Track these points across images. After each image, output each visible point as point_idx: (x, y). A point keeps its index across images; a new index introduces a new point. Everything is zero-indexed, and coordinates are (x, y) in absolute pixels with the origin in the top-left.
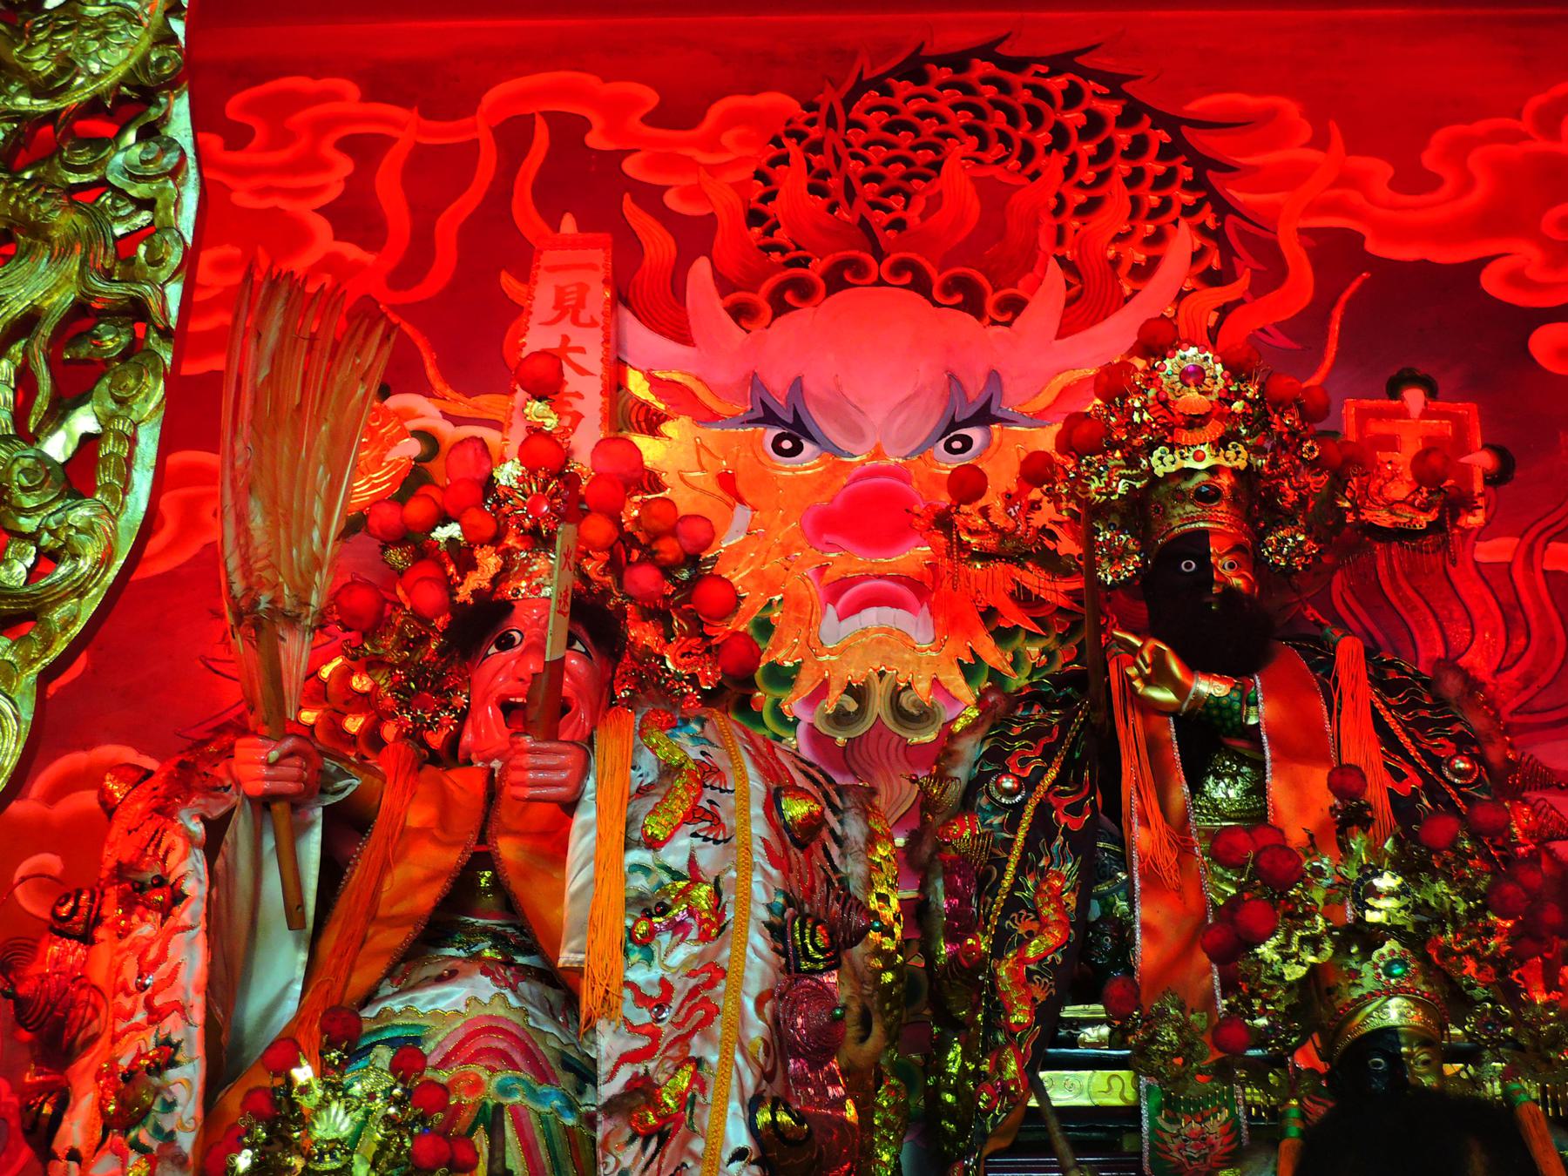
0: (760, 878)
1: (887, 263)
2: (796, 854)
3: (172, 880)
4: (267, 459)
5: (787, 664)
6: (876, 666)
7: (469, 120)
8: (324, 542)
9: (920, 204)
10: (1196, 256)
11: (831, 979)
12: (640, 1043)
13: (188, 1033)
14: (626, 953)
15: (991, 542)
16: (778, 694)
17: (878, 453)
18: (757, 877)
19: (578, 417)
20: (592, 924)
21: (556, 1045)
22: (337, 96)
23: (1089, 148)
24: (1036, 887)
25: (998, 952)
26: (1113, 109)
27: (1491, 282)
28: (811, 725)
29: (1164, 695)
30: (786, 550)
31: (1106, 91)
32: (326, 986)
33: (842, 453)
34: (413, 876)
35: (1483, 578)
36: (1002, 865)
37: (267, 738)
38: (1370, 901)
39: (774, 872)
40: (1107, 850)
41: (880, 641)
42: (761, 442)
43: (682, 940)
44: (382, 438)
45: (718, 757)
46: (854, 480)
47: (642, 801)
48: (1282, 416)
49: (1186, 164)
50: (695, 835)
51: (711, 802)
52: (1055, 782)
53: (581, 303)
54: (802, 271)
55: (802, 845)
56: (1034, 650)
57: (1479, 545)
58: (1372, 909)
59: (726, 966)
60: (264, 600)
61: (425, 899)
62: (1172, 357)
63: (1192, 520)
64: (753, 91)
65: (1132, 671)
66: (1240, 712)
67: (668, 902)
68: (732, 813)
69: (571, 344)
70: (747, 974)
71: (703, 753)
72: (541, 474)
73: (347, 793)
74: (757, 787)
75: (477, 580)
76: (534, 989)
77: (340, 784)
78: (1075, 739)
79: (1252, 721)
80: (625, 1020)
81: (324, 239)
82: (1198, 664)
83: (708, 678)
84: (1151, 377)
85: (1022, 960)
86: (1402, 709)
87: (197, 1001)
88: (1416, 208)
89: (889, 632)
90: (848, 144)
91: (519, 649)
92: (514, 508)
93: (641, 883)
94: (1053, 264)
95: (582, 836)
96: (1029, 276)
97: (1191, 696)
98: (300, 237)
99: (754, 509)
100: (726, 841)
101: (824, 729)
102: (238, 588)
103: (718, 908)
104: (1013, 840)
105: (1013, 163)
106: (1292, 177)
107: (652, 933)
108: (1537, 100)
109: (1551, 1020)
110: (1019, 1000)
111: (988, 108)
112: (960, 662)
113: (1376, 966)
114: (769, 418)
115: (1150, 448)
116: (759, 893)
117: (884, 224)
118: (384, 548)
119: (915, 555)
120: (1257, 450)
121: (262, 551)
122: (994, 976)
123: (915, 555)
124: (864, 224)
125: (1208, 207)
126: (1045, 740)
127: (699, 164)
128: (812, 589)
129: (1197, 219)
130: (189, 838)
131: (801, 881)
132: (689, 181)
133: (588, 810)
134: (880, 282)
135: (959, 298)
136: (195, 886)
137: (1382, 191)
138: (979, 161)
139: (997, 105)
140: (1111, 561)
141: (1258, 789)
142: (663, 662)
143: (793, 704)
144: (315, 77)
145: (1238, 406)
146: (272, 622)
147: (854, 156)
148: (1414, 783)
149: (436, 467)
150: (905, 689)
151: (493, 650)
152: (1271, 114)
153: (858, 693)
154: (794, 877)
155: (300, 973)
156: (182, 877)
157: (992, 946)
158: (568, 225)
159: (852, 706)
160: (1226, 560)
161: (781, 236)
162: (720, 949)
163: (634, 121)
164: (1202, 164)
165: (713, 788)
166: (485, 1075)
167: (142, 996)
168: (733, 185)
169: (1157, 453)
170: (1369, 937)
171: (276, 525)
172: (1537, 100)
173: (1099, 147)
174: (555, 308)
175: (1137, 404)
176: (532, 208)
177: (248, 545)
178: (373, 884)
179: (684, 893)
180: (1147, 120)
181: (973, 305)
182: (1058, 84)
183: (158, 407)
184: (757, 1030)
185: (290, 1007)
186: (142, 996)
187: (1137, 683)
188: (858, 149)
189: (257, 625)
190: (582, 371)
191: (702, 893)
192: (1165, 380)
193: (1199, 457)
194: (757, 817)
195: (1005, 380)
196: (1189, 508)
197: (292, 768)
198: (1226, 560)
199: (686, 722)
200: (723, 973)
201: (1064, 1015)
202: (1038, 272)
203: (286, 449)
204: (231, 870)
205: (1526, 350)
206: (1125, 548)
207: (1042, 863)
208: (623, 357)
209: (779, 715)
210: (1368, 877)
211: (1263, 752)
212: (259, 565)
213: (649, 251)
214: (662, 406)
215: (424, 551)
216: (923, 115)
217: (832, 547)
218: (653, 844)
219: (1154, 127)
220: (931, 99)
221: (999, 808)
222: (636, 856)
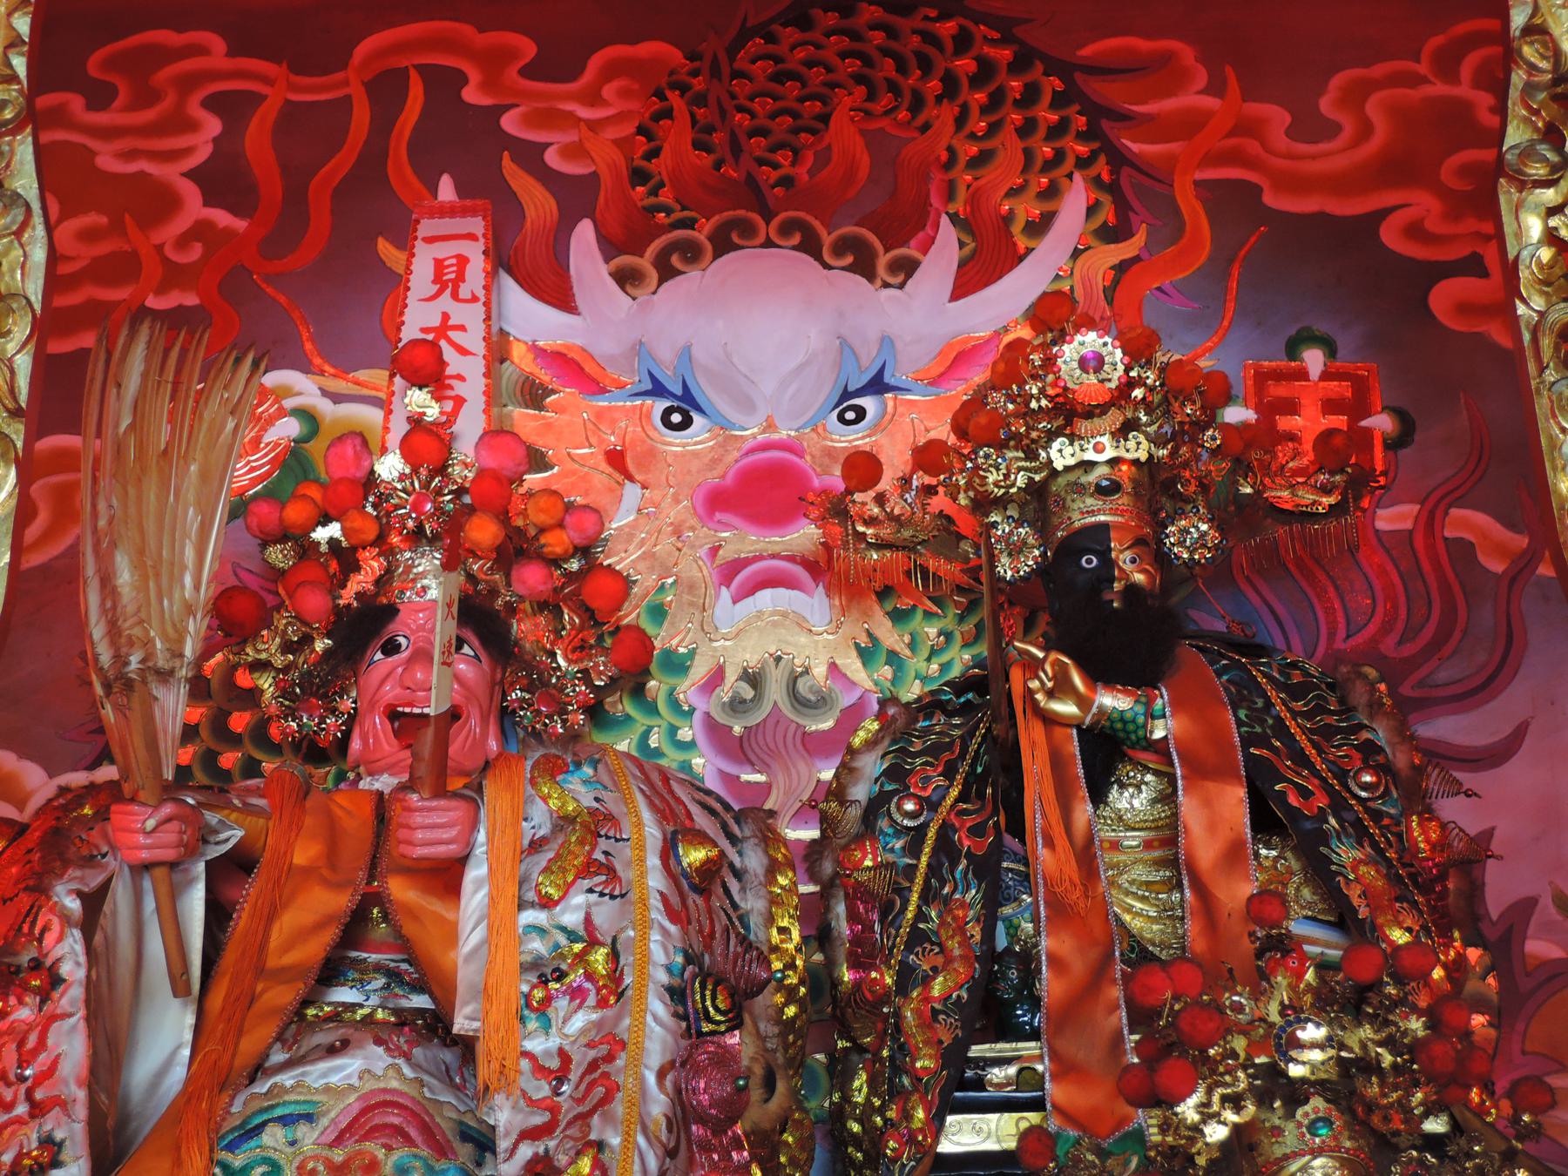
0: (658, 937)
1: (775, 222)
2: (695, 899)
3: (48, 962)
4: (132, 510)
5: (682, 650)
6: (772, 650)
7: (339, 76)
8: (197, 587)
9: (809, 158)
10: (1091, 210)
11: (734, 1039)
12: (539, 1119)
13: (71, 1130)
14: (522, 1020)
15: (886, 532)
16: (672, 681)
17: (770, 426)
18: (655, 936)
19: (459, 401)
20: (485, 993)
21: (454, 1115)
22: (202, 51)
23: (980, 96)
24: (940, 916)
25: (903, 987)
26: (1005, 54)
27: (1390, 236)
28: (707, 715)
29: (1066, 708)
30: (677, 532)
31: (997, 36)
32: (214, 1057)
33: (733, 426)
34: (303, 921)
35: (1384, 547)
36: (904, 893)
37: (144, 804)
38: (1293, 1053)
39: (673, 928)
40: (1011, 870)
41: (775, 624)
42: (649, 415)
43: (580, 1006)
44: (260, 418)
45: (612, 803)
46: (747, 454)
47: (536, 858)
48: (1183, 405)
49: (1079, 113)
50: (591, 891)
51: (606, 853)
52: (957, 800)
53: (461, 277)
54: (689, 232)
55: (703, 891)
56: (932, 631)
57: (1380, 512)
58: (1296, 1061)
59: (625, 1037)
60: (134, 661)
61: (314, 949)
62: (1071, 342)
63: (1092, 513)
64: (634, 41)
65: (1034, 684)
66: (1145, 726)
67: (564, 967)
68: (628, 864)
69: (451, 323)
70: (648, 1044)
71: (597, 799)
72: (423, 472)
73: (229, 845)
74: (653, 832)
75: (360, 582)
76: (429, 1054)
77: (223, 836)
78: (977, 752)
79: (1159, 734)
80: (524, 1093)
81: (194, 208)
82: (1102, 673)
83: (601, 673)
84: (1050, 362)
85: (926, 999)
86: (1308, 715)
87: (81, 1095)
88: (1314, 157)
89: (784, 615)
90: (733, 97)
91: (404, 655)
92: (397, 507)
93: (537, 946)
94: (945, 220)
95: (476, 892)
96: (921, 235)
97: (1094, 710)
98: (164, 202)
99: (644, 487)
100: (622, 896)
101: (721, 718)
102: (105, 658)
103: (615, 976)
104: (916, 867)
105: (903, 115)
106: (1188, 125)
107: (548, 1000)
108: (1437, 41)
109: (1477, 1155)
110: (926, 1043)
111: (876, 55)
112: (857, 645)
113: (1300, 1125)
114: (658, 390)
115: (1051, 436)
116: (658, 953)
117: (772, 181)
118: (264, 545)
119: (805, 535)
120: (1157, 441)
121: (130, 609)
122: (898, 1014)
123: (805, 535)
124: (750, 180)
125: (1102, 159)
126: (946, 756)
127: (580, 119)
128: (705, 572)
129: (1093, 171)
130: (66, 919)
131: (701, 931)
132: (571, 137)
133: (479, 866)
134: (769, 244)
135: (849, 260)
136: (73, 968)
137: (1280, 141)
138: (867, 113)
139: (886, 52)
140: (1010, 555)
141: (1167, 797)
142: (553, 655)
143: (687, 688)
144: (180, 30)
145: (1138, 393)
146: (144, 682)
147: (740, 109)
148: (1321, 802)
149: (317, 448)
150: (802, 674)
151: (379, 656)
152: (1167, 58)
153: (753, 679)
154: (694, 926)
155: (188, 1036)
156: (59, 960)
157: (896, 983)
158: (446, 191)
159: (749, 693)
160: (1128, 555)
161: (666, 197)
162: (619, 1018)
163: (512, 74)
164: (1098, 112)
165: (608, 837)
166: (381, 1153)
167: (23, 1088)
168: (616, 142)
169: (1056, 445)
170: (1296, 1093)
171: (145, 578)
172: (1437, 41)
173: (990, 95)
174: (434, 282)
175: (1035, 391)
176: (408, 171)
177: (114, 607)
178: (261, 932)
179: (581, 957)
180: (1039, 67)
181: (864, 267)
182: (947, 28)
183: (10, 495)
184: (658, 1105)
185: (179, 1073)
186: (23, 1088)
187: (1039, 697)
188: (743, 101)
189: (129, 685)
190: (463, 351)
191: (599, 957)
192: (1063, 367)
193: (1099, 449)
194: (654, 867)
195: (899, 345)
196: (1089, 501)
197: (170, 835)
198: (1128, 555)
199: (578, 765)
200: (623, 1045)
201: (970, 1054)
202: (929, 230)
203: (152, 497)
204: (110, 944)
205: (1425, 298)
206: (1024, 543)
207: (946, 890)
208: (507, 328)
209: (675, 704)
210: (1289, 1024)
211: (1172, 765)
212: (127, 624)
213: (530, 213)
214: (546, 378)
215: (307, 549)
216: (810, 64)
217: (727, 526)
218: (547, 903)
219: (1046, 74)
220: (818, 47)
221: (901, 831)
222: (529, 917)
